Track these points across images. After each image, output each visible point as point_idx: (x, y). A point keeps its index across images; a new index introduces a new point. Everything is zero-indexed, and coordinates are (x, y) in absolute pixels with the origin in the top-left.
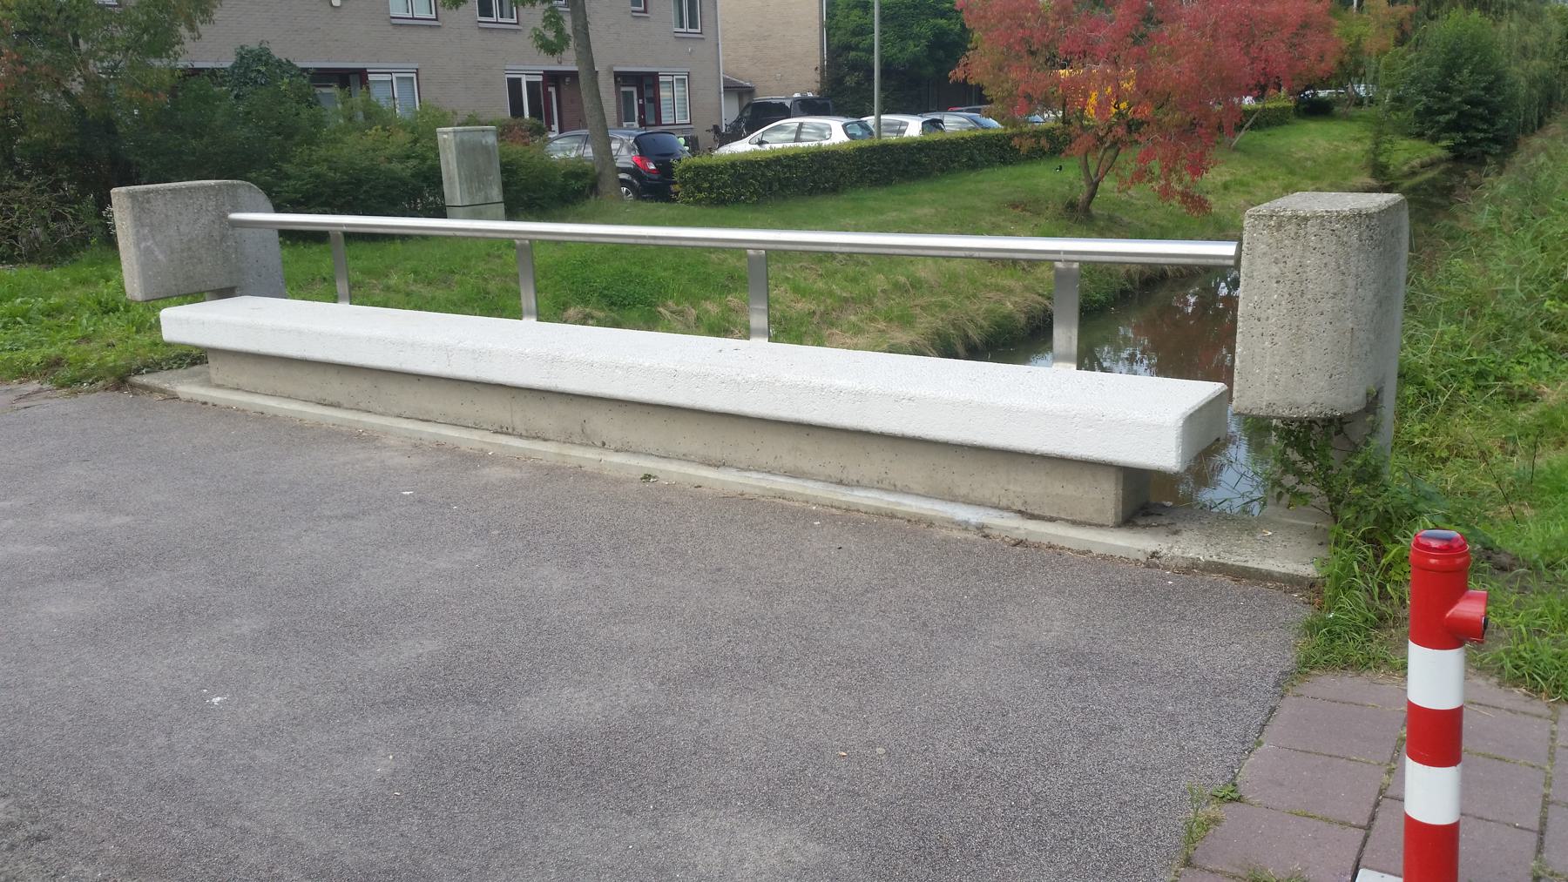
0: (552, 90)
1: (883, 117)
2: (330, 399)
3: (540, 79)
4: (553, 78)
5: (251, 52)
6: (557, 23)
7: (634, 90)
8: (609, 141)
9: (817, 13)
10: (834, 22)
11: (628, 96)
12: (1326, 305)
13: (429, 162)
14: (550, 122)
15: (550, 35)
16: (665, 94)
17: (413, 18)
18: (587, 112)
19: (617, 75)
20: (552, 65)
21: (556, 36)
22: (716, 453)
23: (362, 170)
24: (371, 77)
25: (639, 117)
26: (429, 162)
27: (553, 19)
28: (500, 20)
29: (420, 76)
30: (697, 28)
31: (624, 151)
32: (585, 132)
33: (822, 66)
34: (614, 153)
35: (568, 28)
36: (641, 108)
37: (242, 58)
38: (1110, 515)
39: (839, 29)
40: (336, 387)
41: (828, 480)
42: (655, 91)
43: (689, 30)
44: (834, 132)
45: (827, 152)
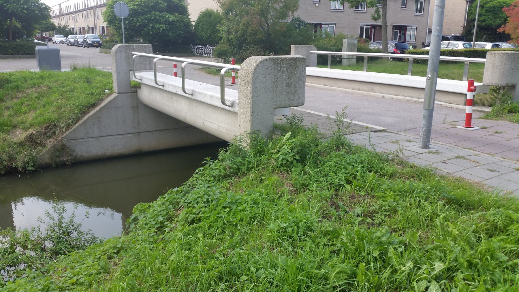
0: (373, 30)
1: (476, 43)
2: (326, 85)
3: (370, 27)
4: (374, 27)
5: (295, 18)
6: (378, 12)
7: (398, 31)
8: (387, 44)
9: (465, 9)
10: (470, 12)
11: (396, 33)
12: (499, 67)
13: (339, 47)
14: (371, 40)
15: (376, 16)
16: (408, 32)
17: (337, 9)
18: (382, 36)
19: (394, 26)
20: (374, 23)
21: (377, 16)
22: (396, 93)
23: (325, 48)
24: (323, 26)
25: (399, 39)
26: (339, 47)
27: (377, 12)
28: (361, 10)
29: (336, 26)
30: (422, 13)
31: (391, 47)
32: (381, 42)
33: (464, 26)
34: (388, 48)
35: (381, 14)
36: (400, 36)
37: (293, 20)
38: (463, 104)
39: (472, 14)
40: (327, 82)
41: (417, 98)
42: (405, 32)
43: (419, 13)
44: (460, 46)
45: (454, 51)
